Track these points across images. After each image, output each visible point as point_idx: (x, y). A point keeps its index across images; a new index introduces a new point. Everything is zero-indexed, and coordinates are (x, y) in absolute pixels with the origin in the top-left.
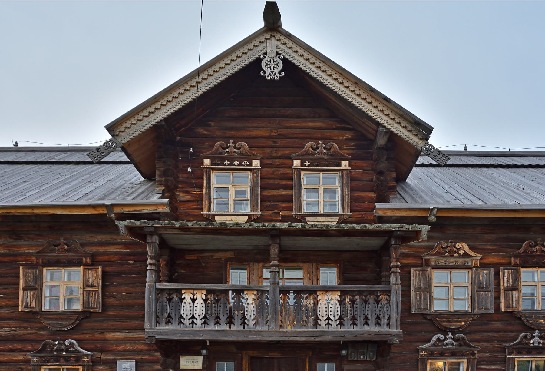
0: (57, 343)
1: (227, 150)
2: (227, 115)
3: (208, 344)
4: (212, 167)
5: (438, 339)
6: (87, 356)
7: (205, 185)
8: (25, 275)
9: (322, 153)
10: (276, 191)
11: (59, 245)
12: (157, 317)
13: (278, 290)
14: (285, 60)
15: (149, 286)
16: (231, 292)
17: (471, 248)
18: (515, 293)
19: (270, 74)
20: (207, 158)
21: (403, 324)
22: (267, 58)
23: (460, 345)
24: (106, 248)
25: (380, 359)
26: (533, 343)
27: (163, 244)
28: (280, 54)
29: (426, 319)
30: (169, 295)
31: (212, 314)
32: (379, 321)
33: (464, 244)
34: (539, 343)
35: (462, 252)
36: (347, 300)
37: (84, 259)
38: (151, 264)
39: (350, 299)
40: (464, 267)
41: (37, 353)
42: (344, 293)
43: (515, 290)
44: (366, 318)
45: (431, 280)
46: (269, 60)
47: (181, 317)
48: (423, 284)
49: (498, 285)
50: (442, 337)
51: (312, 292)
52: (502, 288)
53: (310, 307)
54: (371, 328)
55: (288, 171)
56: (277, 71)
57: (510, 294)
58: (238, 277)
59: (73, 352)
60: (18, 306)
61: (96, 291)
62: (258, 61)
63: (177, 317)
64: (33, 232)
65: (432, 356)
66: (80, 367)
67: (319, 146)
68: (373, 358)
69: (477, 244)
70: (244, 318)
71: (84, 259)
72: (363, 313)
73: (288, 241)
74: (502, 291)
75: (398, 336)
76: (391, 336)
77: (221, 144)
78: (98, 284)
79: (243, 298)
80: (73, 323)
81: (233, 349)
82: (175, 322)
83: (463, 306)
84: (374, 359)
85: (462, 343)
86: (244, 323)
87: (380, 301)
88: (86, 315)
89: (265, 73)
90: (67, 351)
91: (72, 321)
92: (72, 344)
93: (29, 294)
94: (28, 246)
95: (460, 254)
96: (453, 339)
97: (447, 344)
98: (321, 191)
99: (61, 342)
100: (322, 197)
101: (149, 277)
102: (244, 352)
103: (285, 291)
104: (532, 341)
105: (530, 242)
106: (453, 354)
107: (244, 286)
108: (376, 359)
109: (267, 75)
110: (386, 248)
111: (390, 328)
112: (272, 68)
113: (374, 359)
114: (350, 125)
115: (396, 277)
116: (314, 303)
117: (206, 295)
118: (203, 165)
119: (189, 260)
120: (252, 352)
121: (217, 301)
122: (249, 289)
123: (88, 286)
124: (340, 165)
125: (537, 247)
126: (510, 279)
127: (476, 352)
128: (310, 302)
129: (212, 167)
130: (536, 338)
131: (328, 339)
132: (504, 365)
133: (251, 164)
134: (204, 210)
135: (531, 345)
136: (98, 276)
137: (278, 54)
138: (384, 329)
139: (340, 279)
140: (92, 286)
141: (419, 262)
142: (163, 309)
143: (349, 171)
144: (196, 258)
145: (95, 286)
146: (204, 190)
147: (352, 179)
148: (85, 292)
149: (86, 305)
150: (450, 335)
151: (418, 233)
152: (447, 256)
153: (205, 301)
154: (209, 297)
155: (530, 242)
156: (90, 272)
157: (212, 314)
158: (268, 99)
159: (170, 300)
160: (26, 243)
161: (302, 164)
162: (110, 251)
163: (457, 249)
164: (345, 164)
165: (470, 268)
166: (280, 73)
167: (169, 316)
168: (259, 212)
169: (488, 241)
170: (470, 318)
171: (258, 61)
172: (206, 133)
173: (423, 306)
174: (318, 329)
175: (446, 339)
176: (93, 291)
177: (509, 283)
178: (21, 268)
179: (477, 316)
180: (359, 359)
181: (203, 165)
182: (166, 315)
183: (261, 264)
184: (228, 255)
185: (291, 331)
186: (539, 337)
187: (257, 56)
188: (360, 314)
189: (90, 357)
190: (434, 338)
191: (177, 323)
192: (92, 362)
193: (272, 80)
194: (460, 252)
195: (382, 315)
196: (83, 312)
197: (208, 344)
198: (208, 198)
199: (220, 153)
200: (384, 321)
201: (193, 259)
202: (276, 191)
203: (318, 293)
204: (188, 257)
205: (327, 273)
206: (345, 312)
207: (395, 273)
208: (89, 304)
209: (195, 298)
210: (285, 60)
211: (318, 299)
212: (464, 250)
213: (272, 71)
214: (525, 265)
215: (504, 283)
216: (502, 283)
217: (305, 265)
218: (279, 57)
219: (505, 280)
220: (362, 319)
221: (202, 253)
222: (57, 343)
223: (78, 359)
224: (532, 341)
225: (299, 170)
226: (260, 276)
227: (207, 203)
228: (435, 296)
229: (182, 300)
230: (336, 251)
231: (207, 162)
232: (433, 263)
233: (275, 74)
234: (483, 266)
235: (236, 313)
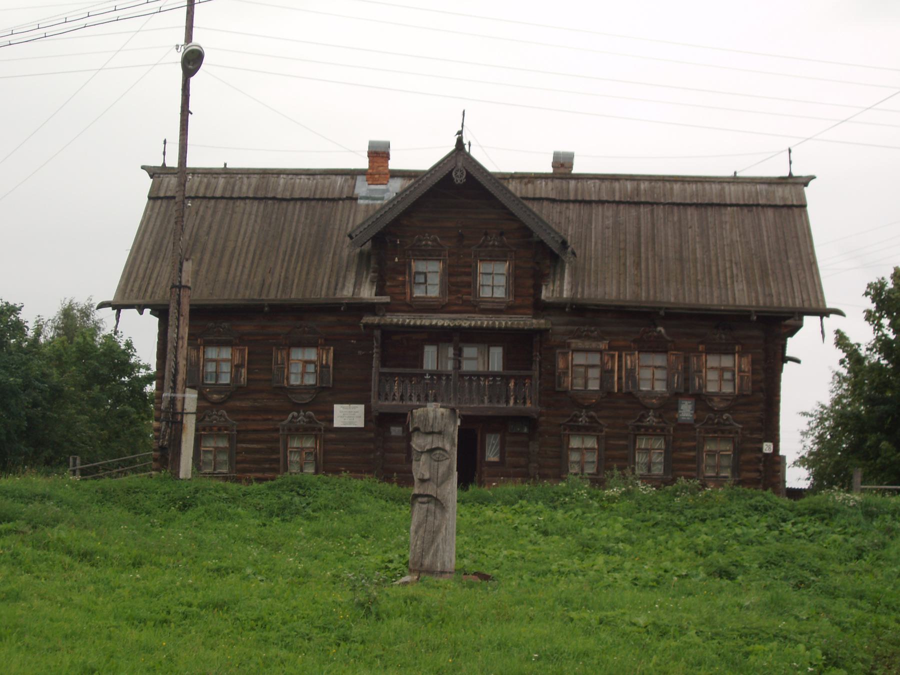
50: (295, 414)
100: (494, 281)
150: (302, 413)
175: (299, 416)
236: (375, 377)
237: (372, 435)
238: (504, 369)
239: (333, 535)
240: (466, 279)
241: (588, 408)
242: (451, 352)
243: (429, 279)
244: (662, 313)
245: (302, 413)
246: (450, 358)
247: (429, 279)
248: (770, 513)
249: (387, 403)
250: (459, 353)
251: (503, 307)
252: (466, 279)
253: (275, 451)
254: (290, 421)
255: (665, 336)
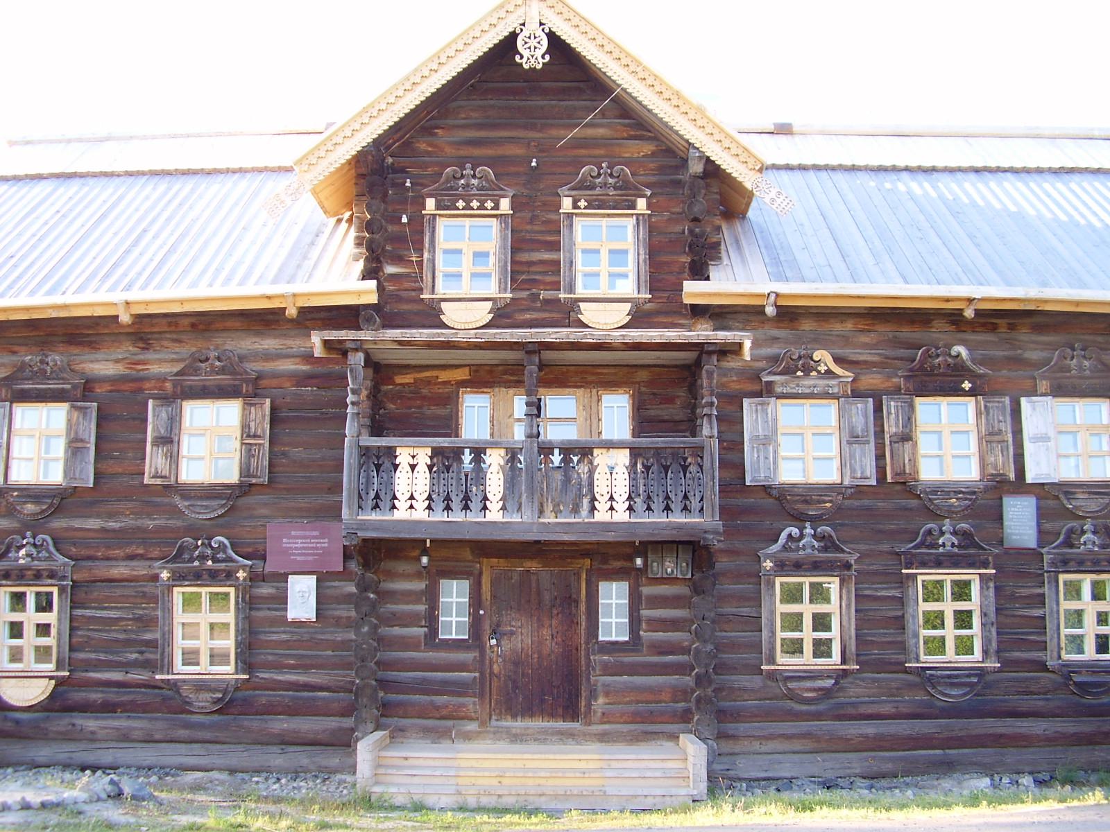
0: (200, 543)
1: (462, 181)
2: (463, 116)
3: (428, 545)
4: (439, 212)
5: (790, 535)
6: (244, 567)
7: (427, 245)
8: (156, 416)
9: (605, 184)
10: (534, 263)
11: (207, 359)
12: (360, 497)
13: (536, 449)
14: (551, 36)
15: (350, 441)
16: (467, 451)
17: (838, 360)
18: (908, 445)
19: (528, 59)
20: (431, 196)
21: (725, 512)
22: (526, 33)
23: (825, 549)
24: (276, 364)
25: (697, 576)
26: (944, 545)
27: (370, 362)
28: (544, 24)
29: (770, 495)
30: (378, 458)
31: (439, 492)
32: (688, 502)
33: (824, 352)
34: (953, 545)
35: (822, 368)
36: (639, 466)
37: (244, 385)
38: (353, 403)
39: (643, 464)
40: (826, 396)
41: (168, 562)
42: (635, 453)
43: (907, 441)
44: (668, 498)
45: (775, 420)
46: (528, 35)
47: (395, 497)
48: (763, 430)
49: (880, 433)
50: (795, 531)
51: (586, 451)
52: (887, 436)
53: (585, 477)
54: (678, 518)
55: (553, 217)
56: (539, 53)
57: (901, 448)
58: (476, 414)
59: (224, 561)
60: (144, 474)
61: (260, 444)
62: (513, 36)
63: (389, 497)
64: (168, 336)
65: (782, 571)
66: (232, 591)
67: (602, 171)
68: (687, 574)
69: (849, 353)
70: (485, 498)
71: (244, 385)
72: (662, 488)
73: (548, 355)
74: (887, 442)
75: (716, 533)
76: (705, 532)
77: (454, 170)
78: (264, 431)
79: (484, 463)
80: (223, 506)
81: (467, 554)
82: (385, 507)
83: (828, 474)
84: (689, 576)
85: (829, 544)
86: (485, 508)
87: (688, 467)
88: (244, 489)
89: (522, 57)
90: (215, 560)
91: (224, 502)
92: (222, 547)
93: (160, 451)
94: (160, 361)
95: (819, 372)
96: (814, 536)
97: (804, 548)
98: (604, 255)
99: (206, 541)
100: (605, 262)
101: (350, 428)
102: (485, 560)
103: (546, 450)
104: (940, 542)
105: (928, 350)
106: (817, 567)
107: (486, 442)
108: (692, 575)
109: (524, 60)
110: (698, 364)
111: (699, 520)
112: (532, 49)
113: (689, 576)
114: (650, 131)
115: (710, 423)
116: (590, 471)
117: (431, 458)
118: (425, 209)
119: (401, 384)
120: (497, 560)
121: (448, 469)
122: (495, 445)
123: (249, 436)
124: (633, 207)
125: (940, 359)
126: (898, 420)
127: (853, 562)
128: (583, 469)
129: (439, 212)
130: (947, 536)
131: (610, 537)
132: (900, 590)
133: (496, 207)
134: (425, 291)
135: (941, 550)
136: (263, 416)
137: (541, 24)
138: (695, 520)
139: (633, 420)
140: (255, 436)
141: (757, 388)
142: (369, 482)
143: (646, 217)
144: (412, 381)
145: (259, 437)
146: (426, 255)
147: (652, 230)
148: (244, 447)
149: (245, 471)
150: (809, 531)
151: (735, 349)
152: (798, 377)
153: (430, 467)
154: (435, 460)
155: (928, 350)
156: (253, 408)
157: (439, 492)
158: (524, 116)
159: (378, 467)
160: (157, 356)
161: (575, 206)
162: (282, 368)
163: (815, 362)
164: (641, 204)
165: (835, 397)
166: (543, 57)
167: (377, 497)
168: (509, 295)
169: (865, 346)
170: (839, 494)
171: (513, 36)
172: (430, 149)
173: (764, 472)
174: (596, 519)
175: (802, 536)
176: (256, 444)
177: (898, 427)
178: (151, 403)
179: (849, 491)
180: (665, 576)
181: (425, 209)
182: (372, 494)
183: (511, 391)
184: (462, 374)
185: (554, 522)
186: (951, 534)
187: (511, 30)
188: (658, 491)
189: (248, 569)
190: (784, 535)
191: (388, 508)
192: (251, 580)
193: (533, 70)
194: (819, 368)
195: (692, 494)
196: (240, 486)
197: (428, 545)
198: (431, 270)
199: (451, 188)
200: (694, 504)
201: (407, 384)
202: (534, 263)
203: (596, 452)
204: (399, 379)
205: (613, 407)
206: (637, 488)
207: (709, 416)
208: (249, 470)
209: (415, 463)
210: (551, 36)
211: (595, 464)
212: (826, 365)
213: (533, 55)
214: (923, 392)
215: (891, 427)
216: (886, 428)
217: (580, 392)
218: (543, 30)
219: (892, 422)
220: (661, 500)
221: (420, 372)
222: (200, 543)
223: (230, 575)
224: (940, 542)
225: (570, 216)
226: (509, 415)
227: (430, 279)
228: (782, 452)
229: (396, 467)
230: (627, 366)
231: (430, 203)
232: (779, 390)
233: (536, 59)
234: (857, 394)
235: (474, 489)
236: (349, 457)
237: (352, 588)
238: (633, 436)
239: (374, 818)
240: (547, 256)
241: (815, 520)
242: (519, 405)
243: (466, 262)
244: (770, 311)
245: (809, 531)
246: (519, 420)
247: (466, 262)
248: (796, 796)
249: (374, 516)
250: (536, 409)
251: (729, 316)
252: (547, 256)
253: (147, 622)
254: (785, 548)
255: (969, 363)
